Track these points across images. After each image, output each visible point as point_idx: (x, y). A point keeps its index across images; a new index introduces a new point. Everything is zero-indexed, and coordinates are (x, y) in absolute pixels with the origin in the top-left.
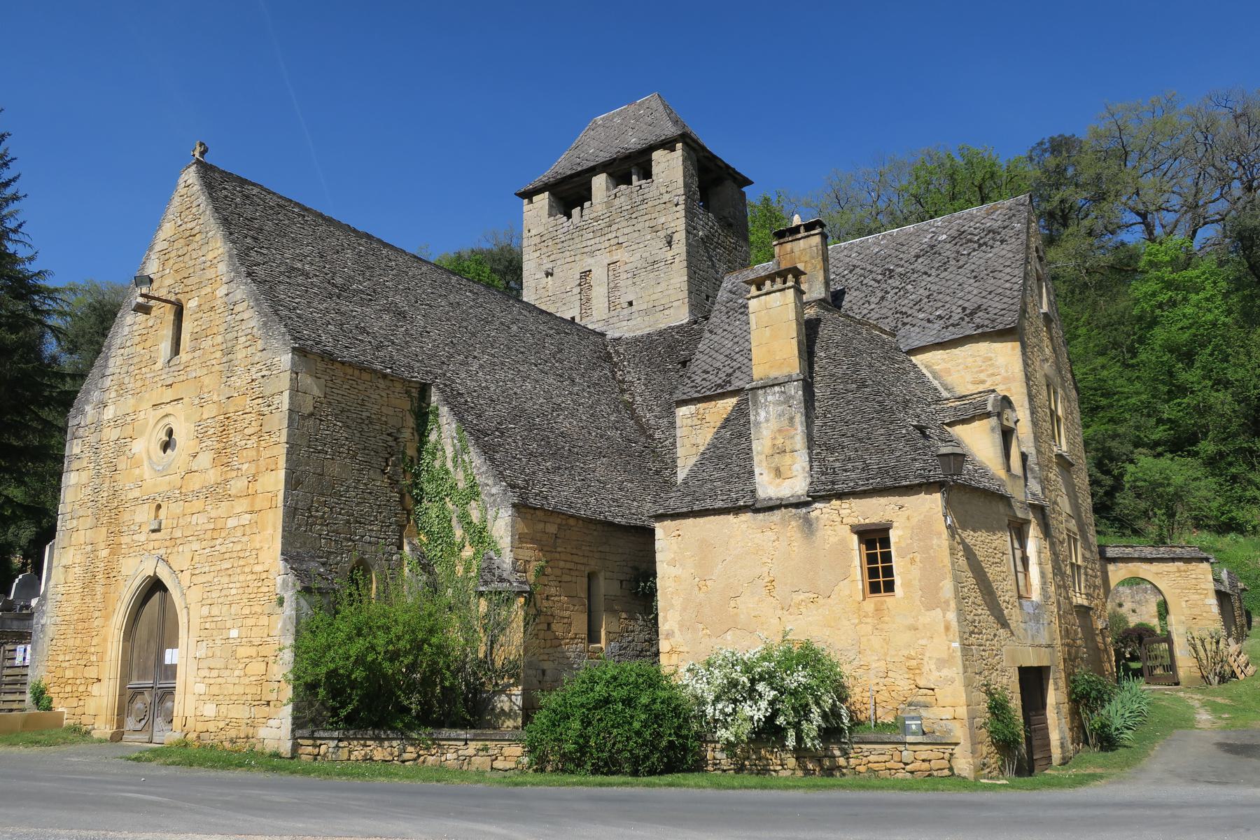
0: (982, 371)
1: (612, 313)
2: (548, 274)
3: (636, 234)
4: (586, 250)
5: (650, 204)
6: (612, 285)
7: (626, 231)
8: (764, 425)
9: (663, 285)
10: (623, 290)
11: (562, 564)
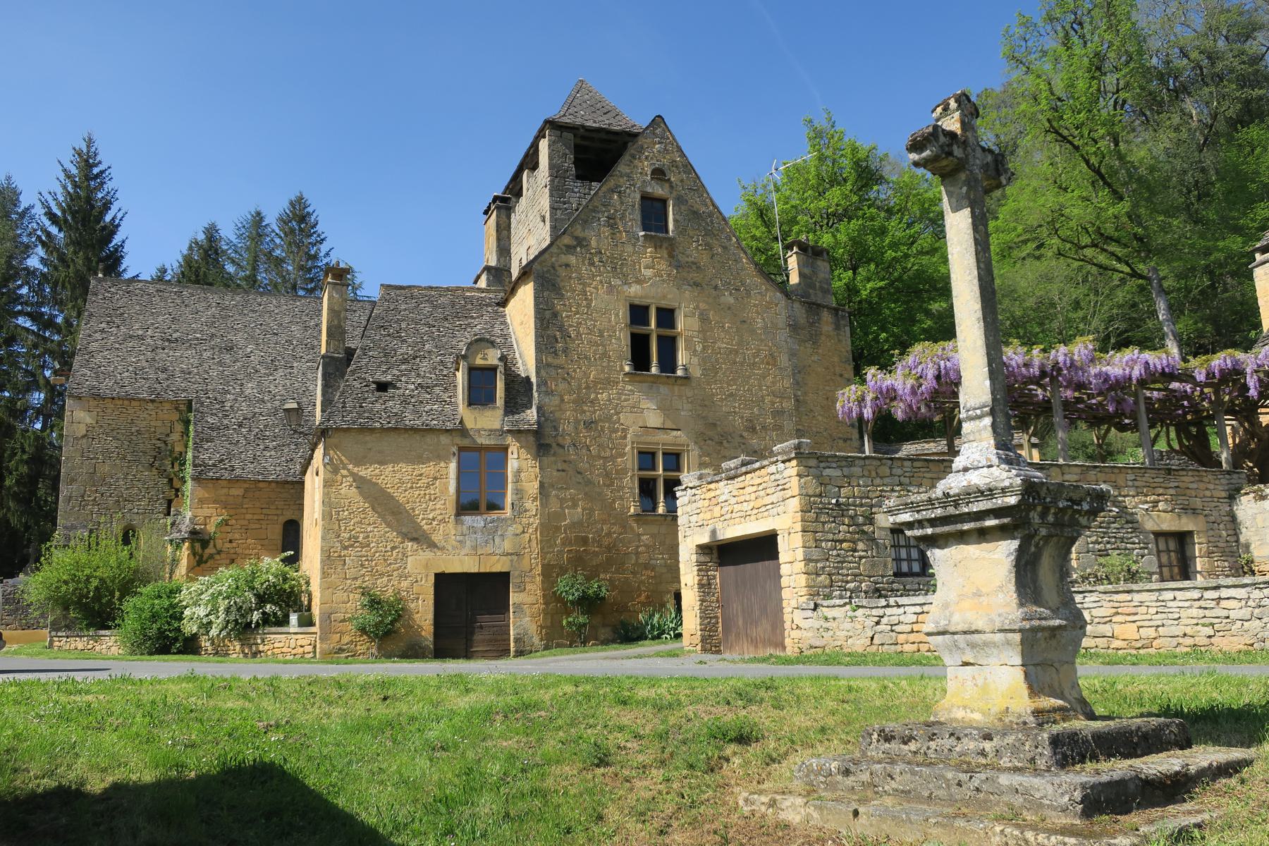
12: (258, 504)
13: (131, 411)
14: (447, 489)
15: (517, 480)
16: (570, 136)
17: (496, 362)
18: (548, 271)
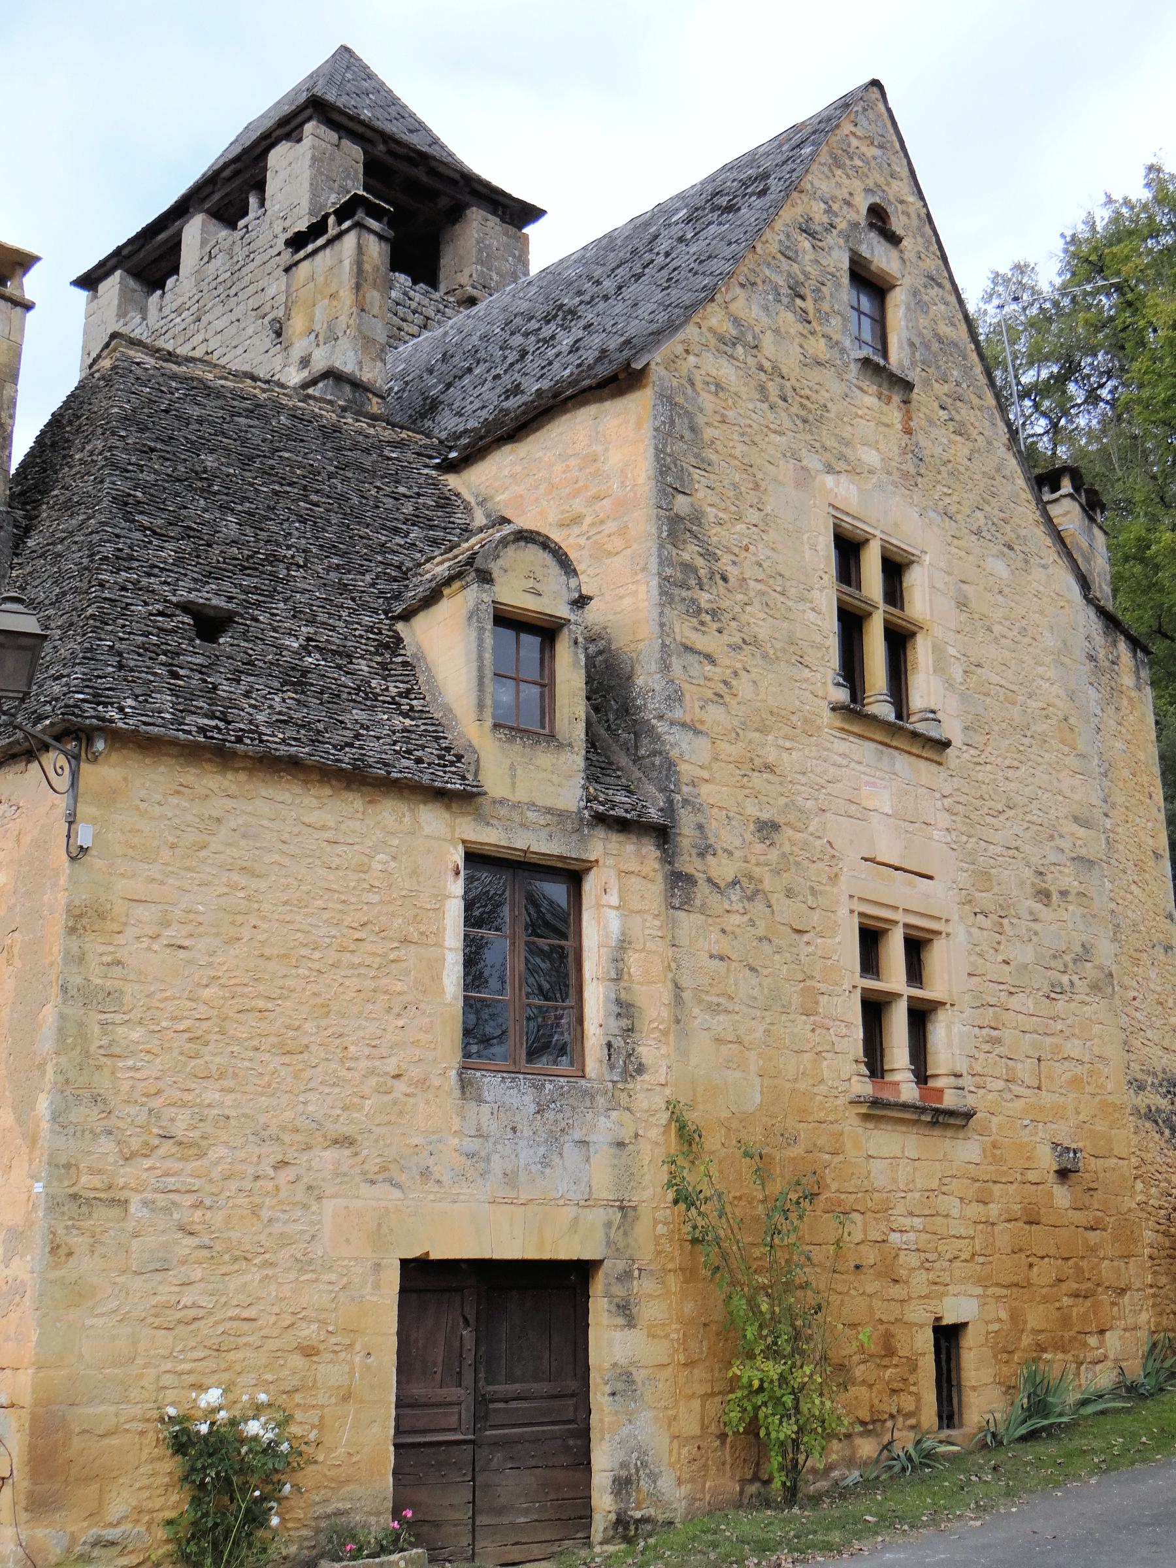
0: (575, 494)
3: (233, 329)
5: (259, 260)
7: (219, 325)
14: (437, 978)
16: (355, 152)
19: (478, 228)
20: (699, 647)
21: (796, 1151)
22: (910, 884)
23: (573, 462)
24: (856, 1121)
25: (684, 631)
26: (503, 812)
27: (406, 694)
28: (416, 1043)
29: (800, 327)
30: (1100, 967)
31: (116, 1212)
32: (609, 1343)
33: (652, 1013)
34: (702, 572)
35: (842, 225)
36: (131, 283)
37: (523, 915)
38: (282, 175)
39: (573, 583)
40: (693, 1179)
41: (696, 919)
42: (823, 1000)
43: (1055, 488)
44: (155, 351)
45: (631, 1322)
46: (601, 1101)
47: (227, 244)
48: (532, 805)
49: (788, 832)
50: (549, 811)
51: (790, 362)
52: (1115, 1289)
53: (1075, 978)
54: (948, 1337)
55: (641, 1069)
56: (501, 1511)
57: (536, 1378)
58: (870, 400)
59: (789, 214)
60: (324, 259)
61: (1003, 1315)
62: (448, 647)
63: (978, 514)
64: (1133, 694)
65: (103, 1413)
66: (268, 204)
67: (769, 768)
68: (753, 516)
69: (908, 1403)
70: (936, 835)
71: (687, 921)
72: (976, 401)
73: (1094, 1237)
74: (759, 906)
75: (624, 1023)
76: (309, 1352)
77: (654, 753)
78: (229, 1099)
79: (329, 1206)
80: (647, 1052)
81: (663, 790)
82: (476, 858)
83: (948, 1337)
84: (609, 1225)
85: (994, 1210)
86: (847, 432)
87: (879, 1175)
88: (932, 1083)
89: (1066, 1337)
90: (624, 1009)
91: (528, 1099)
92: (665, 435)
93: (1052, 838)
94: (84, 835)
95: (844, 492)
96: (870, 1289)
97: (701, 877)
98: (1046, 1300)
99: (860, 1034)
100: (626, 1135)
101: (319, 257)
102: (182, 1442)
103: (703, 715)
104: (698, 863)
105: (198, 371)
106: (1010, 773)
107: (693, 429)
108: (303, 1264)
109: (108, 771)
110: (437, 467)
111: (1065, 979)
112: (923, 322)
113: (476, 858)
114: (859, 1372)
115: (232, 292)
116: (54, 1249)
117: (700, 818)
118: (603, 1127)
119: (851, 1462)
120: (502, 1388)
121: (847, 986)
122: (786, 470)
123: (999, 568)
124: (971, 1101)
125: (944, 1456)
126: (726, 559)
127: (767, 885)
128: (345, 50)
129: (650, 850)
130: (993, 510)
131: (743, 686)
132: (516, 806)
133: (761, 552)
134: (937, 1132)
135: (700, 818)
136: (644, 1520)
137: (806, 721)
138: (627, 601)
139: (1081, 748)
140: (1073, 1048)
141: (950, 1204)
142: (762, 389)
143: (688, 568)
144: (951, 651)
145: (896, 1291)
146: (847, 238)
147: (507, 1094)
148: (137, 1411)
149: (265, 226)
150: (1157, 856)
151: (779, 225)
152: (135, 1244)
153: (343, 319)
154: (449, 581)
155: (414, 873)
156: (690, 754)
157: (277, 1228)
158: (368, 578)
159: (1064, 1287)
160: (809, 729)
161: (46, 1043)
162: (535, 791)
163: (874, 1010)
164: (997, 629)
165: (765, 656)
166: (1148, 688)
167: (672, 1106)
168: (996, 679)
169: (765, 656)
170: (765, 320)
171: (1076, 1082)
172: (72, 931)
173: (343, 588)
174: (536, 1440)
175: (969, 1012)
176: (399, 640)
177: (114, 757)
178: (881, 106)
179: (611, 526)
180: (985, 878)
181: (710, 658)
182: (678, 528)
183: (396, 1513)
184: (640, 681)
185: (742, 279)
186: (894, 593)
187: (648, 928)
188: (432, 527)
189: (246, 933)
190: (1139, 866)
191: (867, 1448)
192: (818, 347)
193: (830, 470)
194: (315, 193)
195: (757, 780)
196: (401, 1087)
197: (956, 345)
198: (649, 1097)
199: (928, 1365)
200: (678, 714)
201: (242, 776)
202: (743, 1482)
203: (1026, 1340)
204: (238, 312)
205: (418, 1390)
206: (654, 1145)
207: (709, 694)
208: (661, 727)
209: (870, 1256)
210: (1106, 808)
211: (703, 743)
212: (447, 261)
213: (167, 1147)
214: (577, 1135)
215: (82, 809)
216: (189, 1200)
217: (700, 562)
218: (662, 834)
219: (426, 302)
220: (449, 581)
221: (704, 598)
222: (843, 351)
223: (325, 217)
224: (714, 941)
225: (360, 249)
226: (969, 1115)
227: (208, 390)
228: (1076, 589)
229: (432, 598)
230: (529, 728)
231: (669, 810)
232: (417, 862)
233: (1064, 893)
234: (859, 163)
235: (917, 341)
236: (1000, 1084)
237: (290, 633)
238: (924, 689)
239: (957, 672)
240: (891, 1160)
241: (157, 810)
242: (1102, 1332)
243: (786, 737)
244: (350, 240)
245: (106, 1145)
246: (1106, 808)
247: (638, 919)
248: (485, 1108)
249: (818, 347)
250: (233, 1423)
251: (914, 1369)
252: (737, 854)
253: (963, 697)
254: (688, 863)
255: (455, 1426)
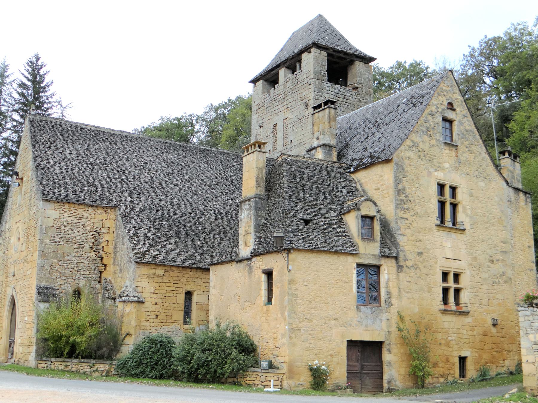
0: (378, 183)
1: (285, 147)
2: (260, 127)
3: (294, 102)
4: (275, 112)
5: (300, 84)
6: (285, 132)
7: (290, 100)
8: (243, 220)
9: (304, 130)
10: (289, 134)
11: (167, 288)
12: (172, 281)
13: (80, 212)
14: (352, 289)
15: (387, 286)
16: (325, 53)
17: (375, 214)
18: (400, 161)
19: (358, 66)
20: (404, 217)
21: (425, 321)
22: (455, 262)
23: (377, 176)
24: (440, 314)
25: (401, 214)
26: (364, 256)
27: (344, 232)
28: (348, 301)
29: (429, 139)
30: (508, 277)
31: (299, 331)
32: (387, 357)
33: (394, 294)
34: (405, 201)
35: (440, 110)
36: (265, 83)
37: (369, 272)
38: (306, 62)
39: (377, 208)
40: (402, 327)
41: (404, 274)
42: (433, 289)
43: (504, 155)
44: (290, 156)
45: (390, 353)
46: (384, 311)
47: (291, 78)
48: (369, 254)
49: (425, 254)
50: (373, 255)
51: (426, 147)
52: (508, 351)
53: (500, 280)
54: (462, 360)
55: (392, 305)
56: (366, 385)
57: (372, 362)
58: (447, 151)
59: (427, 111)
60: (321, 114)
61: (477, 355)
62: (352, 221)
63: (476, 172)
64: (524, 207)
65: (299, 364)
66: (302, 69)
67: (420, 241)
68: (417, 185)
69: (452, 372)
70: (462, 250)
71: (401, 275)
72: (476, 143)
73: (502, 339)
74: (418, 270)
75: (389, 296)
76: (331, 356)
77: (395, 241)
78: (316, 312)
79: (334, 331)
80: (393, 302)
81: (396, 248)
82: (359, 265)
83: (462, 360)
84: (386, 335)
85: (475, 333)
86: (441, 161)
87: (446, 325)
88: (460, 306)
89: (494, 361)
90: (389, 293)
91: (370, 311)
92: (396, 172)
93: (495, 247)
94: (290, 268)
95: (440, 176)
96: (443, 348)
97: (405, 266)
98: (488, 352)
99: (442, 296)
100: (389, 318)
101: (320, 113)
102: (311, 370)
103: (405, 232)
104: (404, 263)
105: (298, 158)
106: (483, 233)
107: (403, 169)
108: (330, 341)
109: (293, 255)
110: (349, 173)
111: (497, 281)
112: (462, 128)
113: (359, 265)
114: (440, 365)
115: (294, 92)
116: (290, 337)
117: (404, 253)
118: (384, 316)
119: (438, 383)
120: (366, 364)
121: (439, 286)
122: (425, 173)
123: (482, 184)
124: (469, 309)
125: (460, 383)
126: (410, 196)
127: (420, 266)
128: (320, 16)
129: (394, 261)
130: (481, 170)
131: (415, 224)
132: (366, 255)
133: (419, 193)
134: (460, 316)
135: (404, 253)
136: (393, 389)
137: (429, 229)
138: (389, 208)
139: (505, 224)
140: (499, 296)
141: (465, 332)
142: (419, 156)
143: (402, 200)
144: (467, 207)
145: (449, 349)
146: (441, 113)
147: (366, 310)
148: (304, 364)
149: (302, 75)
150: (529, 247)
151: (424, 115)
152: (302, 337)
153: (326, 129)
154: (352, 209)
155: (347, 269)
156: (401, 240)
157: (325, 334)
158: (335, 205)
159: (494, 350)
160: (430, 230)
161: (286, 303)
162: (369, 251)
163: (445, 291)
164: (481, 199)
165: (420, 216)
166: (530, 204)
167: (398, 312)
168: (480, 211)
169: (420, 216)
170: (420, 139)
171: (499, 304)
172: (289, 284)
173: (331, 208)
174: (373, 373)
175: (470, 290)
176: (342, 219)
177: (294, 253)
178: (452, 76)
179: (385, 192)
180: (475, 259)
181: (407, 219)
182: (399, 192)
183: (347, 383)
184: (392, 225)
185: (414, 132)
186: (454, 196)
187: (393, 277)
188: (348, 189)
189: (318, 282)
190: (523, 251)
191: (442, 380)
192: (434, 142)
193: (436, 170)
194: (315, 68)
195: (418, 244)
196: (345, 309)
197: (471, 131)
198: (394, 310)
199: (457, 365)
200: (400, 232)
201: (316, 254)
202: (414, 384)
203: (483, 361)
204: (295, 98)
205: (350, 363)
206: (395, 319)
207: (407, 227)
208: (396, 236)
209: (443, 342)
210: (512, 238)
211: (405, 238)
212: (350, 76)
213: (306, 320)
214: (379, 318)
215: (290, 263)
216: (310, 329)
217: (404, 198)
218: (396, 258)
219: (344, 91)
220: (352, 209)
221: (405, 206)
222: (440, 141)
223: (321, 104)
224: (408, 279)
225: (329, 113)
226: (468, 313)
227: (300, 163)
228: (505, 184)
229: (349, 212)
230: (368, 237)
231: (398, 253)
232: (346, 269)
233: (498, 260)
234: (445, 93)
235: (460, 133)
236: (478, 305)
237: (322, 221)
238: (461, 217)
239: (469, 212)
240: (449, 322)
241: (301, 262)
242: (504, 360)
243: (425, 233)
244: (327, 110)
245: (297, 320)
246: (512, 238)
247: (391, 275)
248: (361, 313)
249: (434, 142)
250: (320, 367)
251: (454, 365)
252: (413, 260)
253: (471, 217)
254: (401, 263)
255: (357, 370)
